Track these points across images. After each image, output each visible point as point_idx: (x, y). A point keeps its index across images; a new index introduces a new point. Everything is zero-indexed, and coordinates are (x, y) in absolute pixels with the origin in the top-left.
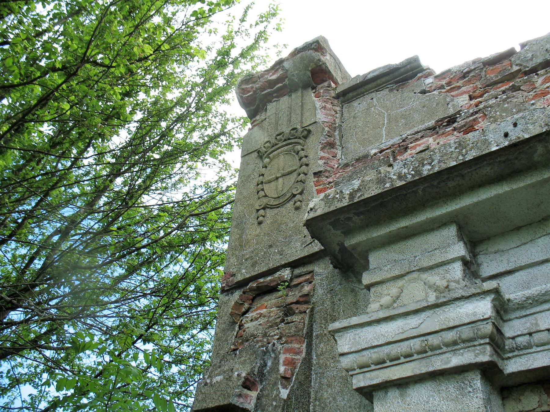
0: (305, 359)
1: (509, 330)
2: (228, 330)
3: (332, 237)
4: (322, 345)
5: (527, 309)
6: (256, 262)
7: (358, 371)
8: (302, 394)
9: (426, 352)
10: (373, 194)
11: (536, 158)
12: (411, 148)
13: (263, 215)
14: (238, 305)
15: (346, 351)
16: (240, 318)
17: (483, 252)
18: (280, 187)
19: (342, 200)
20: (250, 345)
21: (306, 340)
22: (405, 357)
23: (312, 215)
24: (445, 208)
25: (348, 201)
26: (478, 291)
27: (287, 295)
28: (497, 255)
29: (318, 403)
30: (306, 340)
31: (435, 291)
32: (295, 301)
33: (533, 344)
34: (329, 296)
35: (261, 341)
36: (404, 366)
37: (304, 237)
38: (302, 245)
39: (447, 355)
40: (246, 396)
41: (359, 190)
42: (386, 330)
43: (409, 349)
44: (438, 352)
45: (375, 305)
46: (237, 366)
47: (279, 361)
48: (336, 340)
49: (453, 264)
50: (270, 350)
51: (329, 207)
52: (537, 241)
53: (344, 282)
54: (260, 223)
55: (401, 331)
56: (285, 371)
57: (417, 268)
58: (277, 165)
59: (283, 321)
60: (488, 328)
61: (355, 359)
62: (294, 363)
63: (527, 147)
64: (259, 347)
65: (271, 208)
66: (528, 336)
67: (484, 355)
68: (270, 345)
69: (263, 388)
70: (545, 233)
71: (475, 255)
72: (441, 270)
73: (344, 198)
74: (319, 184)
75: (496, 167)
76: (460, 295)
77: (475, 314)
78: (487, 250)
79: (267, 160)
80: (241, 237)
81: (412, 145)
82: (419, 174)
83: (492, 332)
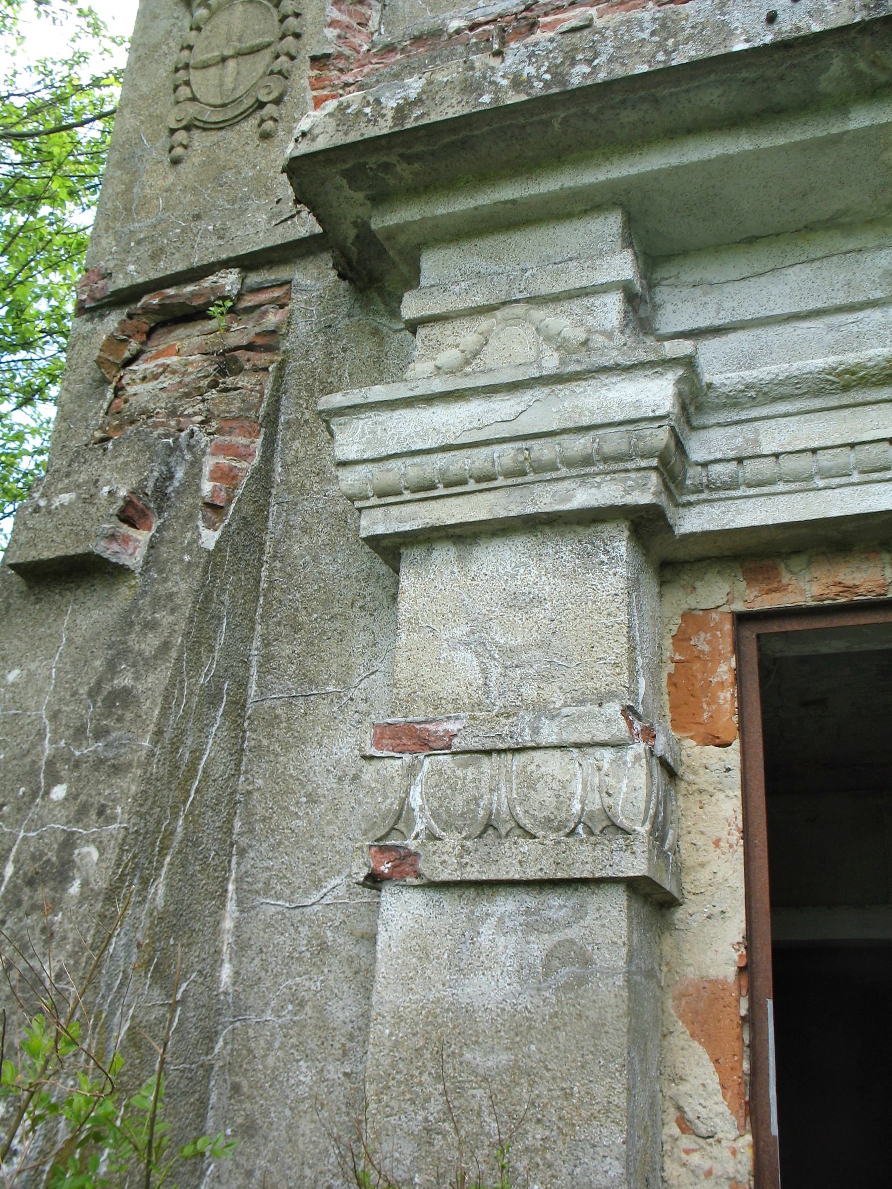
0: (257, 470)
1: (698, 450)
2: (90, 396)
3: (344, 205)
4: (297, 444)
5: (743, 409)
6: (162, 250)
7: (374, 501)
8: (247, 543)
9: (524, 474)
10: (450, 116)
11: (825, 84)
12: (545, 25)
13: (185, 143)
14: (115, 342)
15: (352, 456)
16: (118, 371)
17: (669, 281)
18: (229, 80)
19: (376, 121)
20: (139, 432)
21: (263, 430)
22: (478, 480)
23: (305, 148)
24: (605, 170)
25: (390, 123)
26: (652, 357)
27: (228, 330)
28: (698, 291)
29: (278, 564)
30: (263, 430)
31: (557, 349)
32: (245, 343)
33: (741, 480)
34: (322, 339)
35: (162, 424)
36: (473, 498)
37: (278, 202)
38: (271, 219)
39: (566, 484)
40: (126, 540)
41: (419, 101)
42: (445, 419)
43: (488, 465)
44: (548, 476)
45: (425, 364)
46: (107, 475)
47: (201, 470)
48: (331, 434)
49: (604, 295)
50: (183, 446)
51: (346, 134)
52: (784, 271)
53: (357, 310)
54: (176, 162)
55: (476, 424)
56: (214, 490)
57: (526, 295)
58: (226, 28)
59: (214, 385)
60: (661, 437)
61: (369, 475)
62: (235, 477)
63: (811, 55)
64: (159, 437)
65: (205, 129)
66: (735, 463)
67: (643, 491)
68: (183, 434)
69: (163, 524)
70: (803, 258)
71: (651, 286)
72: (576, 306)
73: (384, 116)
74: (322, 85)
75: (734, 93)
76: (612, 362)
77: (637, 405)
78: (677, 277)
79: (202, 12)
80: (129, 189)
81: (548, 19)
82: (560, 82)
83: (667, 447)
